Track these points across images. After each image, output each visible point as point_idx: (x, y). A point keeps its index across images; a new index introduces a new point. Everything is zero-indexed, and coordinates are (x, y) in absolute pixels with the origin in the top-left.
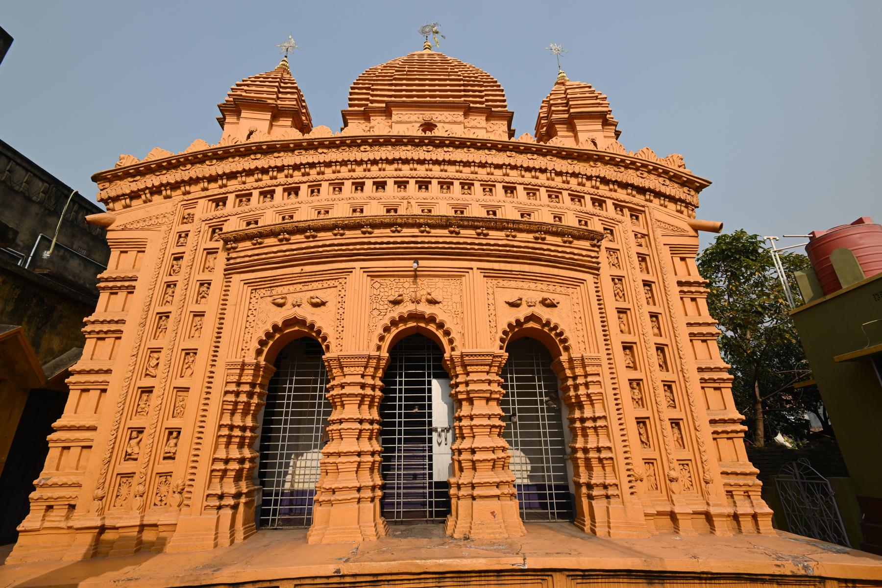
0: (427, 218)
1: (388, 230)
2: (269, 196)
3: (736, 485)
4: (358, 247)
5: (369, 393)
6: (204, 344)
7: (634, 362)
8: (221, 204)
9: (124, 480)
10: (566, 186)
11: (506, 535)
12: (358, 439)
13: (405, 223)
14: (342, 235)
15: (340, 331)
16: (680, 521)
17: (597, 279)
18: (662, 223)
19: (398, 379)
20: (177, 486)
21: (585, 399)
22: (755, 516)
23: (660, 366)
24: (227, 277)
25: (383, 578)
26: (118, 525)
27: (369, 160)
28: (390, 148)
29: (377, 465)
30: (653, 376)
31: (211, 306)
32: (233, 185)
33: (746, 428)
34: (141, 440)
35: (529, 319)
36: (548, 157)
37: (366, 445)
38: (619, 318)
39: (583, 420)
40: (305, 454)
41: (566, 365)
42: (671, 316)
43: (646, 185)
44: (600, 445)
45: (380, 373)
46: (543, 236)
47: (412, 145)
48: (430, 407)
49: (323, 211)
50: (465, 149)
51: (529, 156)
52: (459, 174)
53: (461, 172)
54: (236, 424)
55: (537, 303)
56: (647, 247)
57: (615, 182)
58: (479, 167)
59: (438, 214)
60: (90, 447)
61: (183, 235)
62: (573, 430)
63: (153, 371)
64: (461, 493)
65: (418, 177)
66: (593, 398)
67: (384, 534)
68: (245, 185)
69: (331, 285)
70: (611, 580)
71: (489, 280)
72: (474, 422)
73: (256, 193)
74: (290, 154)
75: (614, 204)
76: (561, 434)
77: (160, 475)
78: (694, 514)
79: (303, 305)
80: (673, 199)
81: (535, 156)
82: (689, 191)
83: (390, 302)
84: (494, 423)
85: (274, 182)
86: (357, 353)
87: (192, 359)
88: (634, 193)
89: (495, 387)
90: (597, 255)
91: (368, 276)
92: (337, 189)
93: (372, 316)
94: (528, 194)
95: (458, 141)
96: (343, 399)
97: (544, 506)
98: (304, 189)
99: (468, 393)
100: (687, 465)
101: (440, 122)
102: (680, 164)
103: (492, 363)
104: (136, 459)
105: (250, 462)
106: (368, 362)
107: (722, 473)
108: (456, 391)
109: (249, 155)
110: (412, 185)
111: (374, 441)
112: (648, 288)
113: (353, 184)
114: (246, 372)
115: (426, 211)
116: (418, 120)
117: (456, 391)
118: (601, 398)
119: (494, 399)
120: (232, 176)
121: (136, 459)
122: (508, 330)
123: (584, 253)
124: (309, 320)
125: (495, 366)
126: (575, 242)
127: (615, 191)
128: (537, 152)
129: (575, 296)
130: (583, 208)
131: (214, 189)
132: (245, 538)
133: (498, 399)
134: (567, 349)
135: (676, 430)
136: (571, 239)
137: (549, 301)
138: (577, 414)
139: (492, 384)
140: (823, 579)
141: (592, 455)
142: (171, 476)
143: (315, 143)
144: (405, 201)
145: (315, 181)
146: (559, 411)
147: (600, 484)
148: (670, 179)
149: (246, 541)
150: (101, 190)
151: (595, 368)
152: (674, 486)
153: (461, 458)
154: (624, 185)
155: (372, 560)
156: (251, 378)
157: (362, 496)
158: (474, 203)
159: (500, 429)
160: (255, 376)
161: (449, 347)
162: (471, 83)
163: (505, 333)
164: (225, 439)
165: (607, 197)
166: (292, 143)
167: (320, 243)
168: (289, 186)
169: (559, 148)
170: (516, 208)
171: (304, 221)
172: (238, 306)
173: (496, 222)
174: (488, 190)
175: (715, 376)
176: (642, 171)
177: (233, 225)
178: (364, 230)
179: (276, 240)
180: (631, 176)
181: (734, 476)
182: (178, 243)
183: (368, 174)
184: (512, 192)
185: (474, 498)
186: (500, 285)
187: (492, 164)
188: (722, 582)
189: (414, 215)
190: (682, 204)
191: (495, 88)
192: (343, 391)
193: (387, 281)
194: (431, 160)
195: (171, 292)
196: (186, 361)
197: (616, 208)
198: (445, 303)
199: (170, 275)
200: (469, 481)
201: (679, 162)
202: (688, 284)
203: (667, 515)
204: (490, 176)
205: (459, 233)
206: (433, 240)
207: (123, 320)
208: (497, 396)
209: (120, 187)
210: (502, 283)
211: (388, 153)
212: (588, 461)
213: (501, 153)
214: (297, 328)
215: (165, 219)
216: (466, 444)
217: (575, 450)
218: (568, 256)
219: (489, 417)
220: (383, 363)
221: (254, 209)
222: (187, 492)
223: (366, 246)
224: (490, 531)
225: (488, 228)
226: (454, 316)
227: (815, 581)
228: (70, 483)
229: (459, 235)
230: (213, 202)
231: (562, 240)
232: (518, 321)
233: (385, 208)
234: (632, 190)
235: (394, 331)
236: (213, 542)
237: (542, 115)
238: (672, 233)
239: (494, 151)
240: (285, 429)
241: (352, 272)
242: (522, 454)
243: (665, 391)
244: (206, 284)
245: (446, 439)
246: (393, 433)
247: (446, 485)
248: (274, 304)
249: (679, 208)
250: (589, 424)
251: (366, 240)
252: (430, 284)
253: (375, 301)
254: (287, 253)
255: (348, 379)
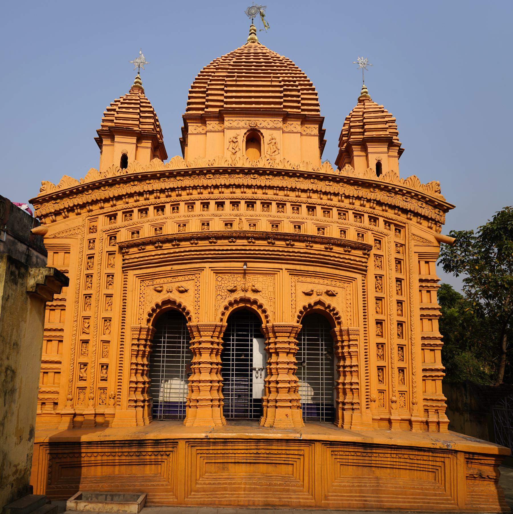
0: (253, 233)
1: (227, 241)
2: (144, 212)
3: (431, 406)
4: (207, 252)
5: (216, 347)
6: (115, 314)
7: (382, 332)
8: (113, 218)
9: (81, 391)
10: (351, 206)
11: (293, 426)
12: (210, 373)
13: (238, 236)
14: (196, 244)
15: (197, 309)
16: (393, 423)
17: (365, 277)
18: (416, 237)
19: (231, 338)
20: (112, 395)
21: (347, 355)
22: (438, 423)
23: (398, 335)
24: (125, 272)
25: (229, 440)
26: (84, 413)
27: (212, 185)
28: (227, 176)
29: (221, 388)
30: (392, 342)
31: (116, 289)
32: (120, 204)
33: (444, 374)
34: (86, 369)
35: (316, 303)
36: (341, 184)
37: (215, 377)
38: (376, 303)
39: (344, 367)
40: (169, 381)
41: (338, 333)
42: (410, 303)
43: (408, 207)
44: (353, 381)
45: (222, 335)
46: (331, 247)
47: (243, 174)
48: (252, 355)
49: (182, 225)
50: (281, 177)
51: (327, 183)
52: (276, 196)
53: (277, 195)
54: (139, 363)
55: (323, 293)
56: (403, 253)
57: (387, 205)
58: (290, 191)
59: (261, 231)
60: (60, 373)
61: (92, 241)
62: (339, 372)
63: (87, 330)
64: (269, 405)
65: (247, 199)
66: (352, 354)
67: (226, 424)
68: (129, 205)
69: (191, 279)
70: (345, 447)
71: (293, 277)
72: (278, 366)
73: (136, 210)
74: (157, 181)
75: (384, 221)
76: (332, 374)
77: (100, 388)
78: (401, 420)
79: (173, 291)
80: (426, 218)
81: (331, 183)
82: (439, 211)
83: (228, 290)
84: (291, 367)
85: (147, 202)
86: (209, 323)
87: (109, 324)
88: (400, 213)
89: (292, 346)
90: (367, 261)
91: (214, 272)
92: (190, 207)
93: (217, 300)
94: (324, 212)
95: (276, 171)
96: (201, 350)
97: (318, 414)
98: (168, 208)
99: (276, 349)
100: (404, 394)
101: (263, 128)
102: (436, 190)
103: (291, 331)
104: (86, 380)
105: (148, 384)
106: (215, 329)
107: (424, 399)
108: (268, 348)
109: (129, 182)
110: (243, 205)
111: (219, 375)
112: (399, 283)
113: (201, 203)
114: (142, 333)
115: (252, 225)
116: (245, 126)
117: (268, 348)
118: (357, 354)
119: (292, 353)
120: (119, 198)
121: (86, 380)
122: (303, 311)
123: (358, 259)
124: (178, 301)
125: (293, 333)
126: (353, 251)
127: (386, 211)
128: (333, 180)
129: (348, 289)
130: (362, 225)
131: (108, 207)
132: (150, 423)
133: (294, 353)
134: (339, 323)
135: (401, 374)
136: (350, 249)
137: (331, 292)
138: (342, 363)
139: (291, 344)
140: (456, 452)
141: (347, 386)
142: (106, 389)
143: (175, 173)
144: (238, 218)
145: (175, 201)
146: (332, 361)
147: (350, 402)
148: (426, 203)
149: (151, 424)
150: (36, 210)
151: (356, 336)
152: (394, 405)
153: (270, 386)
154: (393, 207)
155: (223, 433)
156: (145, 336)
157: (214, 404)
158: (286, 221)
159: (294, 371)
160: (147, 335)
161: (265, 321)
162: (290, 88)
163: (301, 312)
164: (134, 371)
165: (380, 216)
166: (159, 174)
167: (182, 250)
168: (158, 205)
169: (348, 177)
170: (315, 224)
171: (172, 234)
172: (134, 292)
173: (300, 236)
174: (296, 208)
175: (432, 342)
176: (407, 196)
177: (124, 236)
178: (211, 240)
179: (153, 247)
180: (398, 201)
181: (432, 401)
182: (89, 247)
183: (212, 196)
184: (313, 210)
185: (276, 407)
186: (300, 280)
187: (300, 189)
188: (403, 450)
189: (245, 231)
190: (433, 222)
191: (310, 92)
192: (201, 346)
193: (226, 276)
194: (256, 185)
195: (90, 281)
196: (106, 325)
197: (385, 224)
198: (263, 292)
199: (87, 269)
200: (274, 398)
201: (436, 188)
202: (427, 281)
203: (387, 420)
204: (298, 198)
205: (274, 244)
206: (257, 248)
207: (64, 299)
208: (294, 351)
209: (48, 208)
210: (302, 279)
211: (226, 180)
212: (344, 390)
213: (307, 180)
214: (169, 306)
215: (79, 230)
216: (273, 378)
217: (338, 384)
218: (346, 261)
219: (288, 363)
220: (224, 329)
221: (136, 223)
222: (118, 398)
223: (212, 252)
224: (285, 424)
225: (294, 240)
226: (269, 300)
227: (452, 452)
228: (52, 391)
229: (275, 245)
230: (108, 217)
231: (344, 250)
232: (310, 305)
233: (224, 223)
234: (398, 211)
235: (231, 309)
236: (135, 423)
237: (344, 133)
238: (421, 244)
239: (302, 178)
240: (163, 366)
241: (203, 270)
242: (309, 385)
243: (399, 350)
244: (111, 276)
245: (261, 375)
246: (229, 370)
247: (261, 400)
248: (155, 290)
249: (430, 225)
250: (347, 369)
251: (212, 248)
252: (254, 278)
253: (218, 290)
254: (161, 256)
255: (203, 339)
